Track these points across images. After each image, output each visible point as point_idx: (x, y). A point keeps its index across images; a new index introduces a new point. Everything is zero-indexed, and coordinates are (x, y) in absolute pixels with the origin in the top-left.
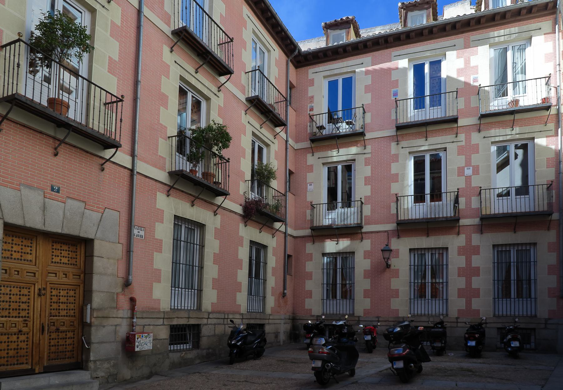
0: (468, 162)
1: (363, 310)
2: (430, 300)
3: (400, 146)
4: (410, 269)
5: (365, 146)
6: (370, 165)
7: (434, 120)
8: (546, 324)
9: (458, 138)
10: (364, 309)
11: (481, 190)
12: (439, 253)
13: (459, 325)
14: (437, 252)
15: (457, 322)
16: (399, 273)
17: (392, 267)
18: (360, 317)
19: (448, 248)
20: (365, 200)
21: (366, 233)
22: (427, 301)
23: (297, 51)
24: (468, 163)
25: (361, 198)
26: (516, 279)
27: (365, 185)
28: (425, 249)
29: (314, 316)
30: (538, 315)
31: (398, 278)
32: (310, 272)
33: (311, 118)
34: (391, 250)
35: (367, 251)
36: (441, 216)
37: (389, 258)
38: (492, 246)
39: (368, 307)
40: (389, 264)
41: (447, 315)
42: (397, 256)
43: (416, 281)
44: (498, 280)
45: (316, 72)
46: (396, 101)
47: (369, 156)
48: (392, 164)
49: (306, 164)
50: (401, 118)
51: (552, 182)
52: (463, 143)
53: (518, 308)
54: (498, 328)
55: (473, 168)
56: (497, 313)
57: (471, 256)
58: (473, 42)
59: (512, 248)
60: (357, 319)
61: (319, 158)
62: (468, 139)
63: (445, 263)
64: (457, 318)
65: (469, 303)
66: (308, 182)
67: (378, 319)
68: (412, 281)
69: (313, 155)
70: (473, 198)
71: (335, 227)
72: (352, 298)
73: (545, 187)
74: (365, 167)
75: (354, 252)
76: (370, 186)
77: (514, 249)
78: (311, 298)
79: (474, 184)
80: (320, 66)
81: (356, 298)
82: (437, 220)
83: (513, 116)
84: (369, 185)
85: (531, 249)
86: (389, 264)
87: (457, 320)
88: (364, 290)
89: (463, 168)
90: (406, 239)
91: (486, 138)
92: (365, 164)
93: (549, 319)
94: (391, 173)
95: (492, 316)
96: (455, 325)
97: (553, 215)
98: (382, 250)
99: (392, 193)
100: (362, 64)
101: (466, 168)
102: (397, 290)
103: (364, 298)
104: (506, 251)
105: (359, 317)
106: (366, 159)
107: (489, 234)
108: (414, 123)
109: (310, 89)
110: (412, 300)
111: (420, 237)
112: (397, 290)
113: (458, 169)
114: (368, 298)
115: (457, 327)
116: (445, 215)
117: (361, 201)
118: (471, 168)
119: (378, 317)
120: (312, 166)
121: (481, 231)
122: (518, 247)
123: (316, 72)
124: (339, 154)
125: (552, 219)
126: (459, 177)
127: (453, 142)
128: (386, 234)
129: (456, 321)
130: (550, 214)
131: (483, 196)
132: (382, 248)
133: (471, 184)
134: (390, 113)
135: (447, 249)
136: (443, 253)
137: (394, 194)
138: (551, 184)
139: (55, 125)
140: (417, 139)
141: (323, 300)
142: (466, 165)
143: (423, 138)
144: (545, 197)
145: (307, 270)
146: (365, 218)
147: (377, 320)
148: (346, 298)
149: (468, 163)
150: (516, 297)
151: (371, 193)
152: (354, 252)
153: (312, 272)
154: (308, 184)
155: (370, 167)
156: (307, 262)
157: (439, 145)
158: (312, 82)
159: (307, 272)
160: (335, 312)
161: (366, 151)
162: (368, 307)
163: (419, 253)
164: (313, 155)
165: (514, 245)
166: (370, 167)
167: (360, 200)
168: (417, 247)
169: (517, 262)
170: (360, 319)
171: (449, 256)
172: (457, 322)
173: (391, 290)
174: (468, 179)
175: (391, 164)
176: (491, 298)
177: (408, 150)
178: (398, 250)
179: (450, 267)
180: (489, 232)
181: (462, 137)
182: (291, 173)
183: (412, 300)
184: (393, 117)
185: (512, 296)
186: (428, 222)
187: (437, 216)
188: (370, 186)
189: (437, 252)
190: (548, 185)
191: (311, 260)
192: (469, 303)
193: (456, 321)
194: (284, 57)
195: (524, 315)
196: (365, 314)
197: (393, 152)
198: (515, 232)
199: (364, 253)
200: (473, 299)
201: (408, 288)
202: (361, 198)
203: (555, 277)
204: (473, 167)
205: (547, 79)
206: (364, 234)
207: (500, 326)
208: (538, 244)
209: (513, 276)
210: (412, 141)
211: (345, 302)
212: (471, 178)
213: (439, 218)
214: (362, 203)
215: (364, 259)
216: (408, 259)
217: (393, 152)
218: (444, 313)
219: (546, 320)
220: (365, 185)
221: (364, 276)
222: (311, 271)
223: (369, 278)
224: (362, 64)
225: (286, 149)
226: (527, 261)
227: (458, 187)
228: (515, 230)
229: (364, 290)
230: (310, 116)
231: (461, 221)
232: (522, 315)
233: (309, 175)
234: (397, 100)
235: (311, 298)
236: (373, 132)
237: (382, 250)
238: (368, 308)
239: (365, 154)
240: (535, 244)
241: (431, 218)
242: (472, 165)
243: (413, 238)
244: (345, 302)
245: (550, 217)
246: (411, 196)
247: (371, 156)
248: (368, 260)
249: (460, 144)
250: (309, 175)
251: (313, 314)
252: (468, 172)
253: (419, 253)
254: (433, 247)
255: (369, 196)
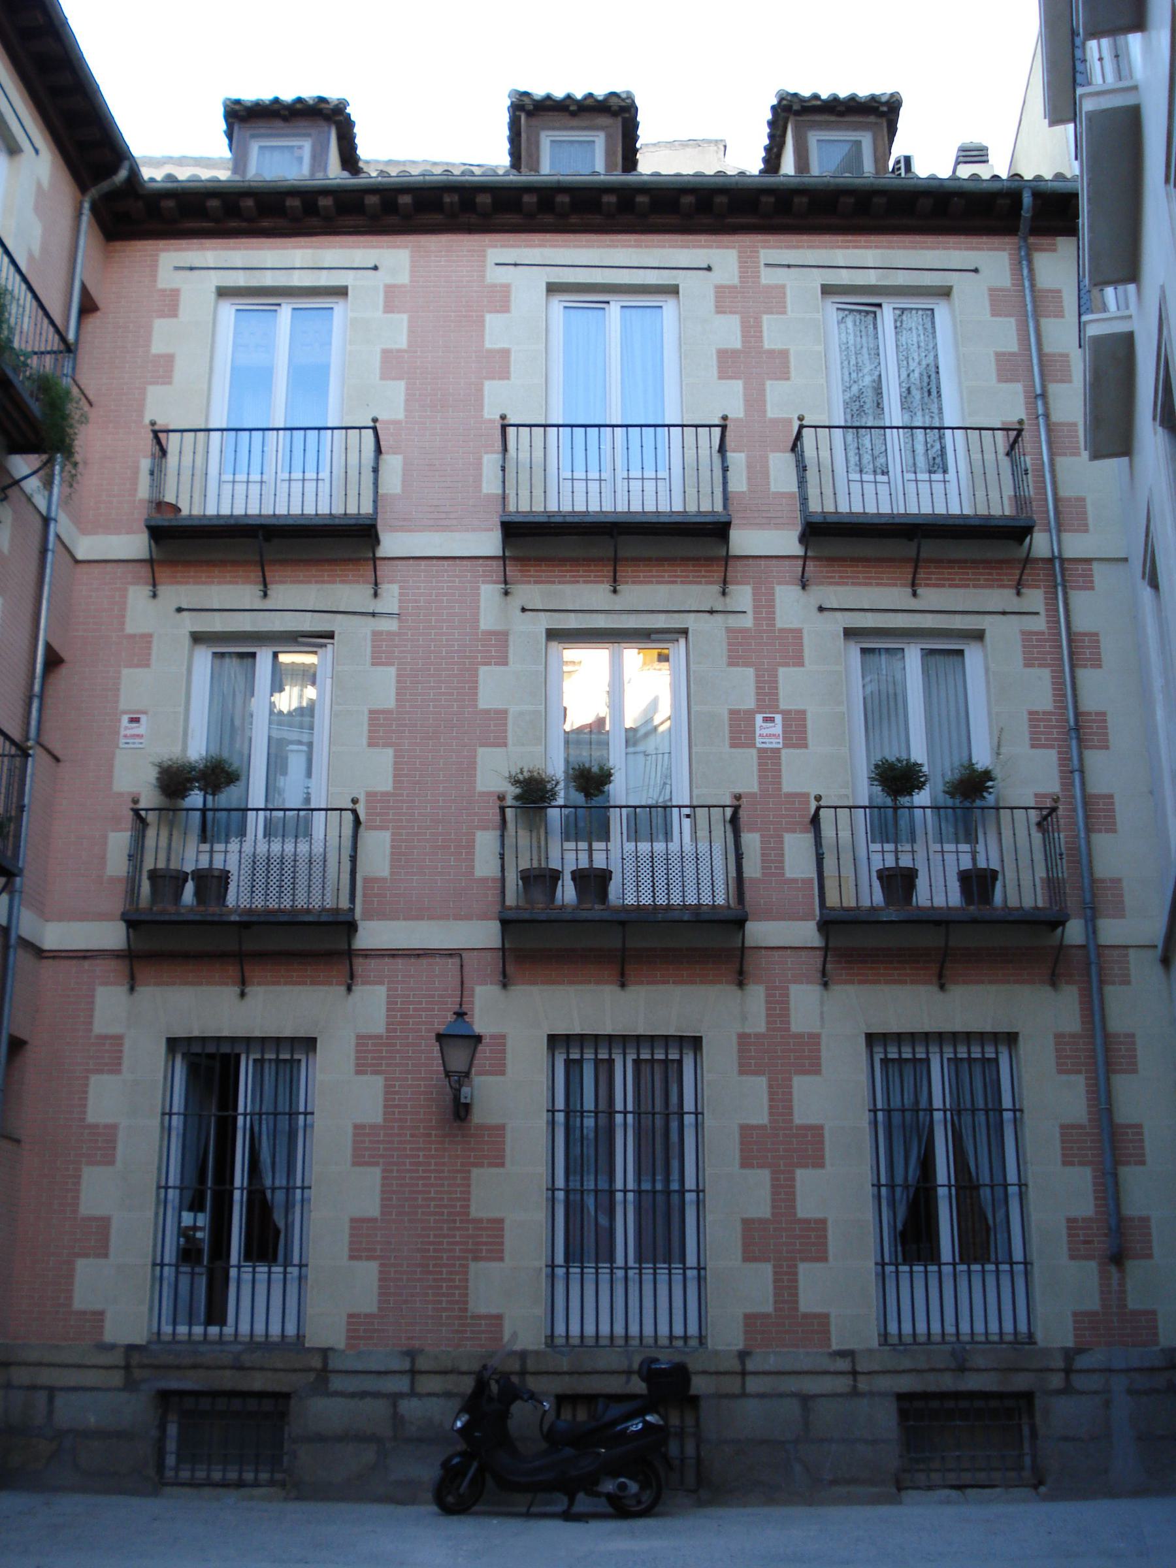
0: (765, 694)
1: (345, 1318)
2: (631, 1273)
3: (516, 601)
4: (553, 1123)
5: (376, 584)
6: (392, 664)
7: (644, 519)
8: (1068, 1371)
9: (728, 600)
10: (350, 1316)
11: (818, 808)
12: (597, 1062)
13: (753, 1385)
14: (589, 1055)
15: (744, 1373)
16: (504, 1143)
17: (478, 1116)
18: (330, 1354)
19: (701, 1037)
20: (367, 808)
21: (368, 954)
22: (620, 1273)
23: (123, 174)
24: (767, 697)
25: (355, 801)
26: (953, 1182)
27: (370, 745)
28: (610, 1038)
29: (112, 1347)
30: (1039, 1336)
31: (502, 1165)
32: (106, 1126)
33: (159, 442)
34: (478, 1039)
35: (370, 1037)
36: (676, 900)
37: (467, 1074)
38: (862, 1041)
39: (368, 1303)
40: (463, 1100)
41: (701, 1339)
42: (499, 1069)
43: (646, 1186)
44: (892, 1187)
45: (191, 269)
46: (504, 427)
47: (391, 625)
48: (483, 670)
49: (123, 630)
50: (524, 493)
51: (1056, 800)
52: (747, 622)
53: (681, 1305)
54: (901, 1397)
55: (784, 720)
56: (893, 1328)
57: (790, 1080)
58: (769, 269)
59: (934, 1049)
60: (316, 1363)
61: (180, 610)
62: (765, 607)
63: (689, 1105)
64: (743, 1355)
65: (786, 1286)
66: (122, 706)
67: (413, 1362)
68: (560, 1182)
69: (154, 596)
70: (788, 838)
71: (237, 919)
72: (296, 1260)
73: (1034, 816)
74: (374, 668)
75: (314, 1040)
76: (390, 752)
77: (625, 1055)
78: (106, 1256)
79: (790, 784)
80: (208, 249)
81: (315, 1260)
82: (660, 917)
83: (913, 545)
84: (386, 745)
85: (1000, 1056)
86: (463, 1100)
87: (743, 1363)
88: (353, 1220)
89: (749, 716)
90: (535, 990)
91: (826, 614)
92: (373, 658)
93: (1079, 1351)
94: (476, 706)
95: (874, 1343)
96: (732, 1385)
97: (1068, 925)
98: (440, 1037)
99: (480, 787)
100: (375, 268)
101: (759, 718)
102: (104, 1224)
103: (352, 1258)
104: (666, 1062)
105: (325, 1352)
106: (376, 634)
107: (851, 989)
108: (569, 519)
109: (160, 325)
110: (560, 1272)
111: (592, 987)
112: (104, 1224)
113: (731, 719)
114: (368, 1258)
115: (744, 1395)
116: (691, 900)
117: (354, 812)
118: (778, 718)
119: (411, 1354)
120: (147, 638)
121: (824, 973)
122: (610, 1050)
123: (191, 269)
124: (268, 604)
125: (747, 944)
126: (733, 750)
127: (711, 612)
128: (452, 964)
129: (737, 1367)
130: (1057, 923)
131: (827, 831)
132: (442, 1029)
133: (780, 783)
134: (479, 465)
135: (696, 1043)
136: (680, 1062)
137: (489, 794)
138: (1054, 810)
139: (748, 173)
140: (578, 582)
141: (162, 1265)
142: (758, 706)
143: (602, 582)
144: (1039, 856)
145: (91, 1118)
146: (364, 888)
147: (406, 1365)
148: (983, 1259)
149: (767, 697)
150: (957, 1260)
151: (394, 782)
152: (314, 1040)
153: (115, 1127)
154: (125, 719)
155: (392, 671)
156: (94, 1079)
157: (662, 617)
158: (170, 304)
159: (90, 1126)
160: (275, 1330)
161: (379, 606)
162: (368, 1303)
163: (946, 1056)
164: (154, 596)
165: (940, 1038)
166: (392, 671)
167: (350, 806)
168: (578, 1031)
169: (958, 1111)
170: (331, 1366)
171: (708, 1077)
172: (744, 1373)
173: (468, 1221)
174: (769, 761)
175: (477, 670)
176: (870, 1265)
177: (545, 622)
178: (503, 1037)
179: (709, 1121)
180: (852, 982)
181: (742, 596)
182: (53, 661)
183: (560, 1272)
184: (490, 485)
185: (946, 1253)
186: (623, 923)
187: (662, 901)
188: (390, 752)
189: (589, 1055)
190: (1045, 812)
191: (115, 1066)
192: (786, 1286)
193: (737, 1367)
194: (65, 189)
195: (178, 1338)
196: (353, 1335)
197: (488, 621)
198: (942, 987)
199: (358, 1045)
200: (803, 1268)
201: (541, 1216)
202: (355, 801)
203: (1087, 1173)
204: (786, 714)
205: (1013, 434)
206: (361, 960)
207: (906, 1384)
208: (1021, 1038)
209: (943, 1171)
210: (560, 586)
211: (262, 1276)
212: (779, 758)
213: (669, 907)
214: (357, 822)
215: (358, 1072)
216: (543, 1079)
217: (488, 621)
218: (693, 1330)
219: (1069, 1355)
220: (370, 745)
221: (354, 1156)
222: (110, 1120)
223: (376, 1164)
224: (375, 268)
225: (44, 551)
226: (990, 1106)
227: (738, 790)
228: (622, 975)
229: (353, 1220)
230: (156, 433)
231: (749, 926)
232: (232, 1339)
233: (129, 675)
234: (506, 422)
235: (106, 1256)
236: (410, 531)
237: (440, 1037)
238: (368, 1311)
239: (373, 614)
240: (1011, 1039)
241: (639, 908)
242: (783, 706)
243: (561, 987)
244: (262, 1276)
245: (1060, 930)
246: (724, 807)
247: (400, 627)
248: (375, 1077)
249: (734, 621)
250: (129, 675)
251: (109, 1337)
252: (769, 733)
253: (949, 1053)
254: (641, 1031)
255: (386, 794)
